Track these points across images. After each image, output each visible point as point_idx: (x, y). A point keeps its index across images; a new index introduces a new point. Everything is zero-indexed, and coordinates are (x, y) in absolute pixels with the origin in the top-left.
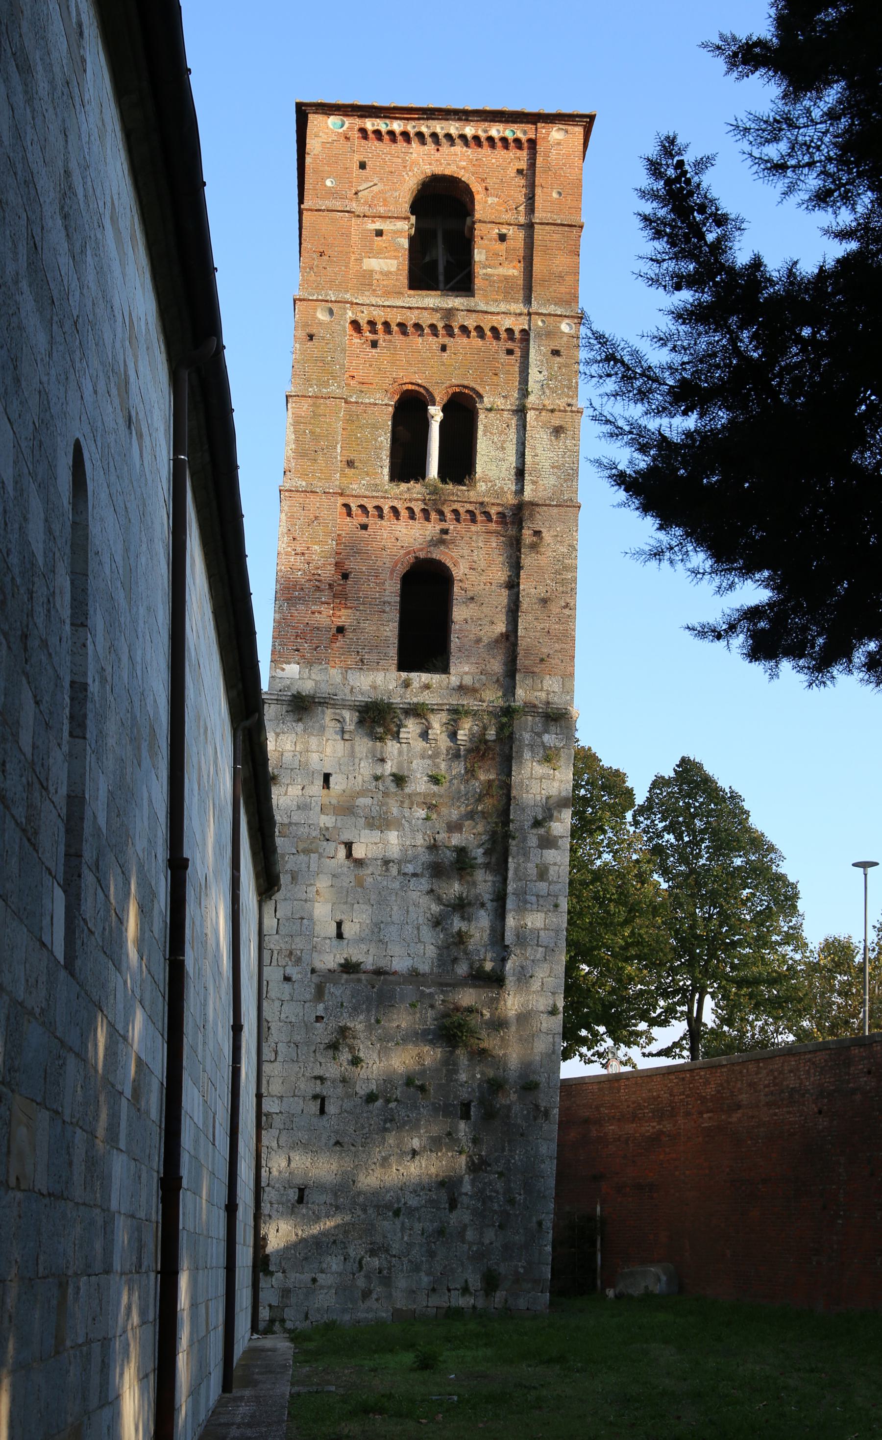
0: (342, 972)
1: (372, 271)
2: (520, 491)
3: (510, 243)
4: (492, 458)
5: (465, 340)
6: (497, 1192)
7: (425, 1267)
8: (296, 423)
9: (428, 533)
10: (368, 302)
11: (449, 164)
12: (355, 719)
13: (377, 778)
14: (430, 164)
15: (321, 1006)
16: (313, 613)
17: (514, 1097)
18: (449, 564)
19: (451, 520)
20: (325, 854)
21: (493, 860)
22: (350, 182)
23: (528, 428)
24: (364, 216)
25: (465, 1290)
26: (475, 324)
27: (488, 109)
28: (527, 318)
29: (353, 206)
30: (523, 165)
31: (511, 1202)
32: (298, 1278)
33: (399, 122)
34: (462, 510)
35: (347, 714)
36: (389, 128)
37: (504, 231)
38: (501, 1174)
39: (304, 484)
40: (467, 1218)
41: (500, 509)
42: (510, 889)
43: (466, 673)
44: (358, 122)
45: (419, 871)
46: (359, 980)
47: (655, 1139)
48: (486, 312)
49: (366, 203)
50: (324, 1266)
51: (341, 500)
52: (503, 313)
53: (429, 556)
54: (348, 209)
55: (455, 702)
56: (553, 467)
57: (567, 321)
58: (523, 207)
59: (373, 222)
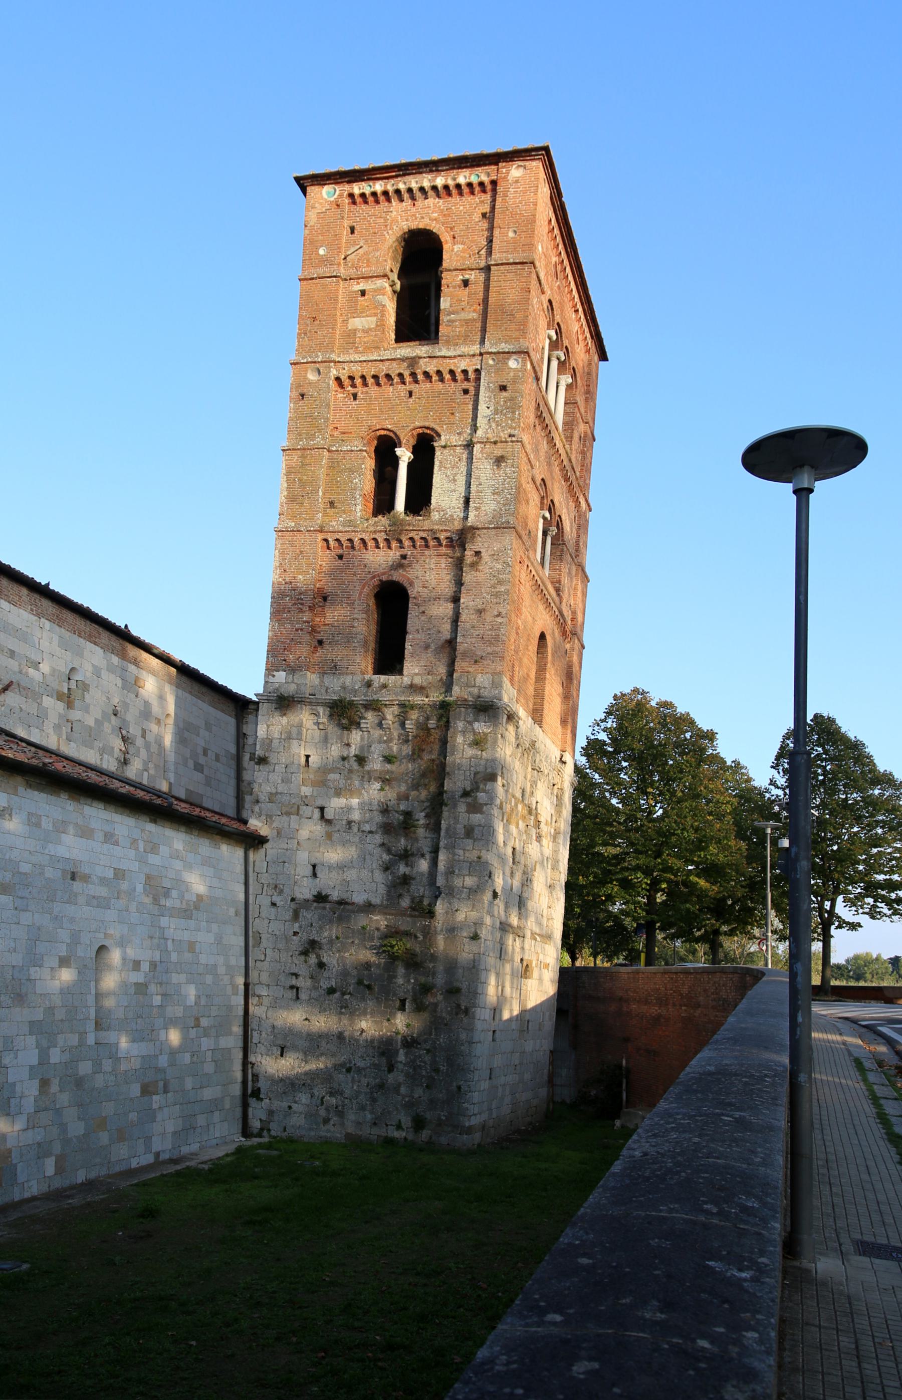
0: (314, 901)
1: (355, 330)
2: (466, 518)
3: (472, 287)
4: (445, 493)
5: (428, 385)
6: (425, 1063)
7: (368, 1108)
8: (289, 473)
9: (390, 559)
10: (348, 359)
11: (423, 218)
12: (327, 713)
13: (344, 759)
14: (407, 220)
15: (297, 925)
16: (297, 630)
17: (440, 998)
18: (406, 585)
19: (409, 547)
20: (305, 816)
21: (432, 821)
22: (339, 248)
23: (474, 460)
24: (350, 279)
25: (399, 1127)
26: (435, 369)
27: (451, 156)
28: (480, 358)
29: (342, 272)
30: (486, 208)
31: (437, 1070)
32: (279, 1104)
33: (380, 182)
34: (416, 538)
35: (321, 710)
36: (372, 190)
37: (467, 277)
38: (428, 1051)
39: (293, 524)
40: (401, 1078)
41: (449, 534)
42: (442, 844)
43: (416, 674)
44: (346, 188)
45: (374, 829)
46: (324, 908)
47: (657, 1019)
48: (445, 357)
49: (353, 266)
50: (297, 1099)
51: (320, 537)
52: (459, 356)
53: (390, 578)
54: (335, 274)
55: (402, 698)
56: (494, 494)
57: (515, 357)
58: (484, 250)
59: (358, 283)
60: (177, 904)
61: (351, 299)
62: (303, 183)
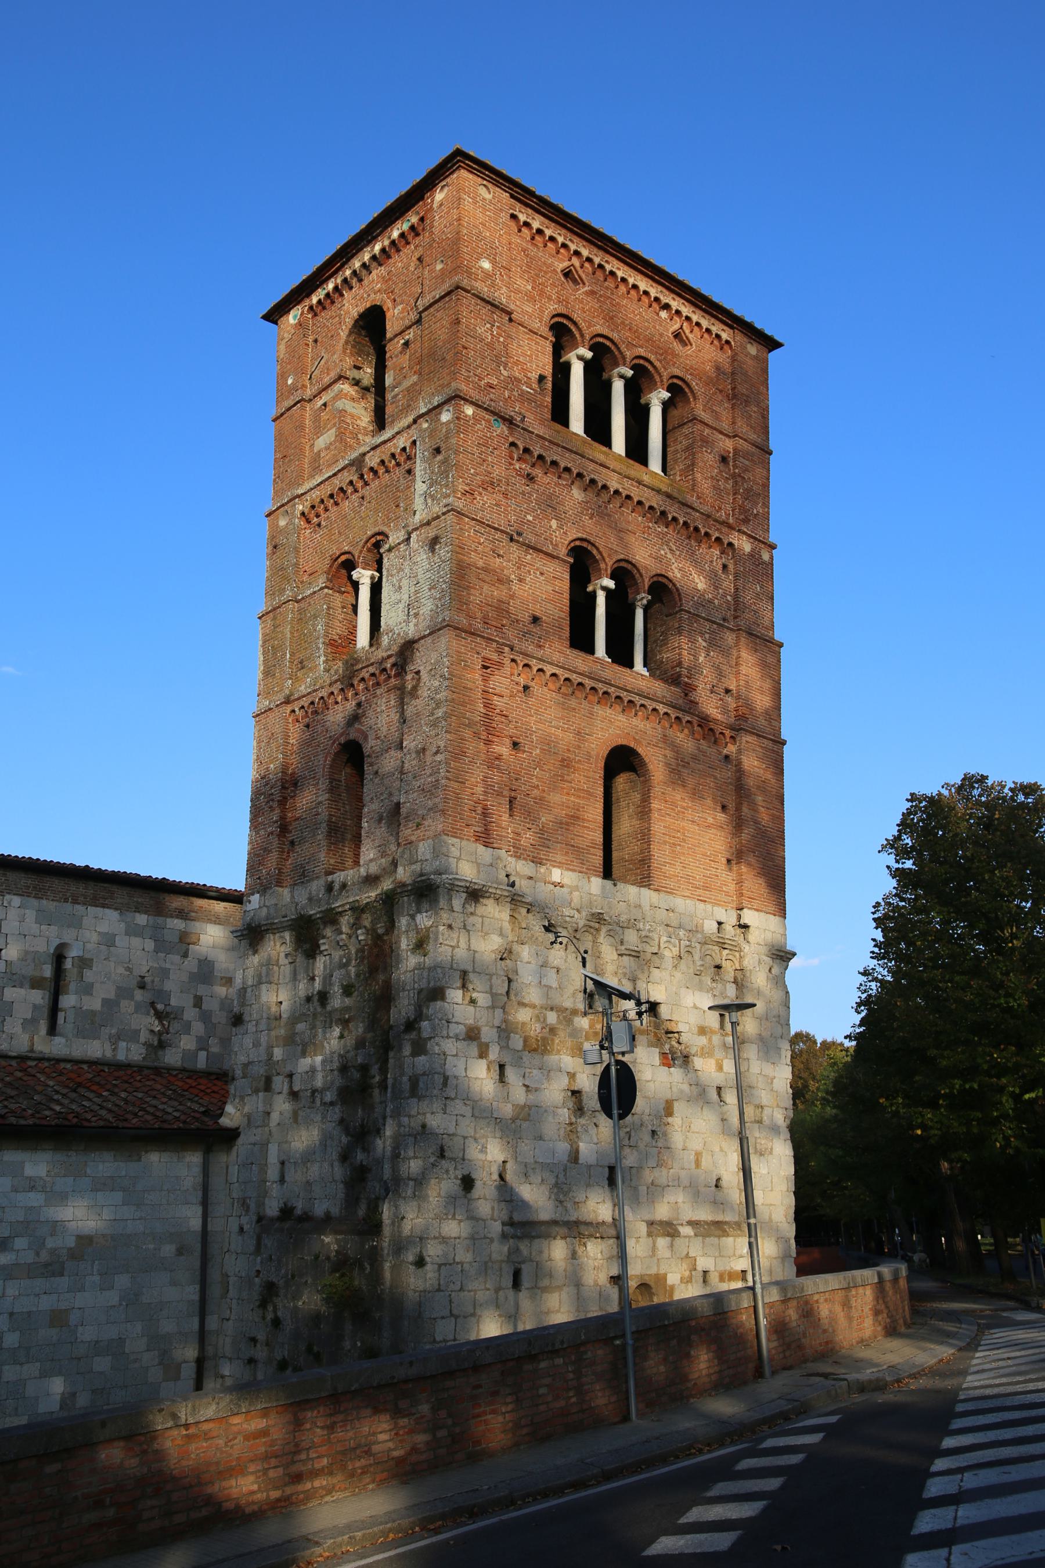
55: (351, 900)
60: (29, 1257)
61: (316, 419)
62: (274, 315)
